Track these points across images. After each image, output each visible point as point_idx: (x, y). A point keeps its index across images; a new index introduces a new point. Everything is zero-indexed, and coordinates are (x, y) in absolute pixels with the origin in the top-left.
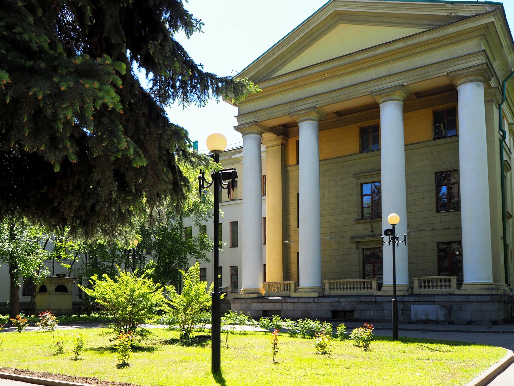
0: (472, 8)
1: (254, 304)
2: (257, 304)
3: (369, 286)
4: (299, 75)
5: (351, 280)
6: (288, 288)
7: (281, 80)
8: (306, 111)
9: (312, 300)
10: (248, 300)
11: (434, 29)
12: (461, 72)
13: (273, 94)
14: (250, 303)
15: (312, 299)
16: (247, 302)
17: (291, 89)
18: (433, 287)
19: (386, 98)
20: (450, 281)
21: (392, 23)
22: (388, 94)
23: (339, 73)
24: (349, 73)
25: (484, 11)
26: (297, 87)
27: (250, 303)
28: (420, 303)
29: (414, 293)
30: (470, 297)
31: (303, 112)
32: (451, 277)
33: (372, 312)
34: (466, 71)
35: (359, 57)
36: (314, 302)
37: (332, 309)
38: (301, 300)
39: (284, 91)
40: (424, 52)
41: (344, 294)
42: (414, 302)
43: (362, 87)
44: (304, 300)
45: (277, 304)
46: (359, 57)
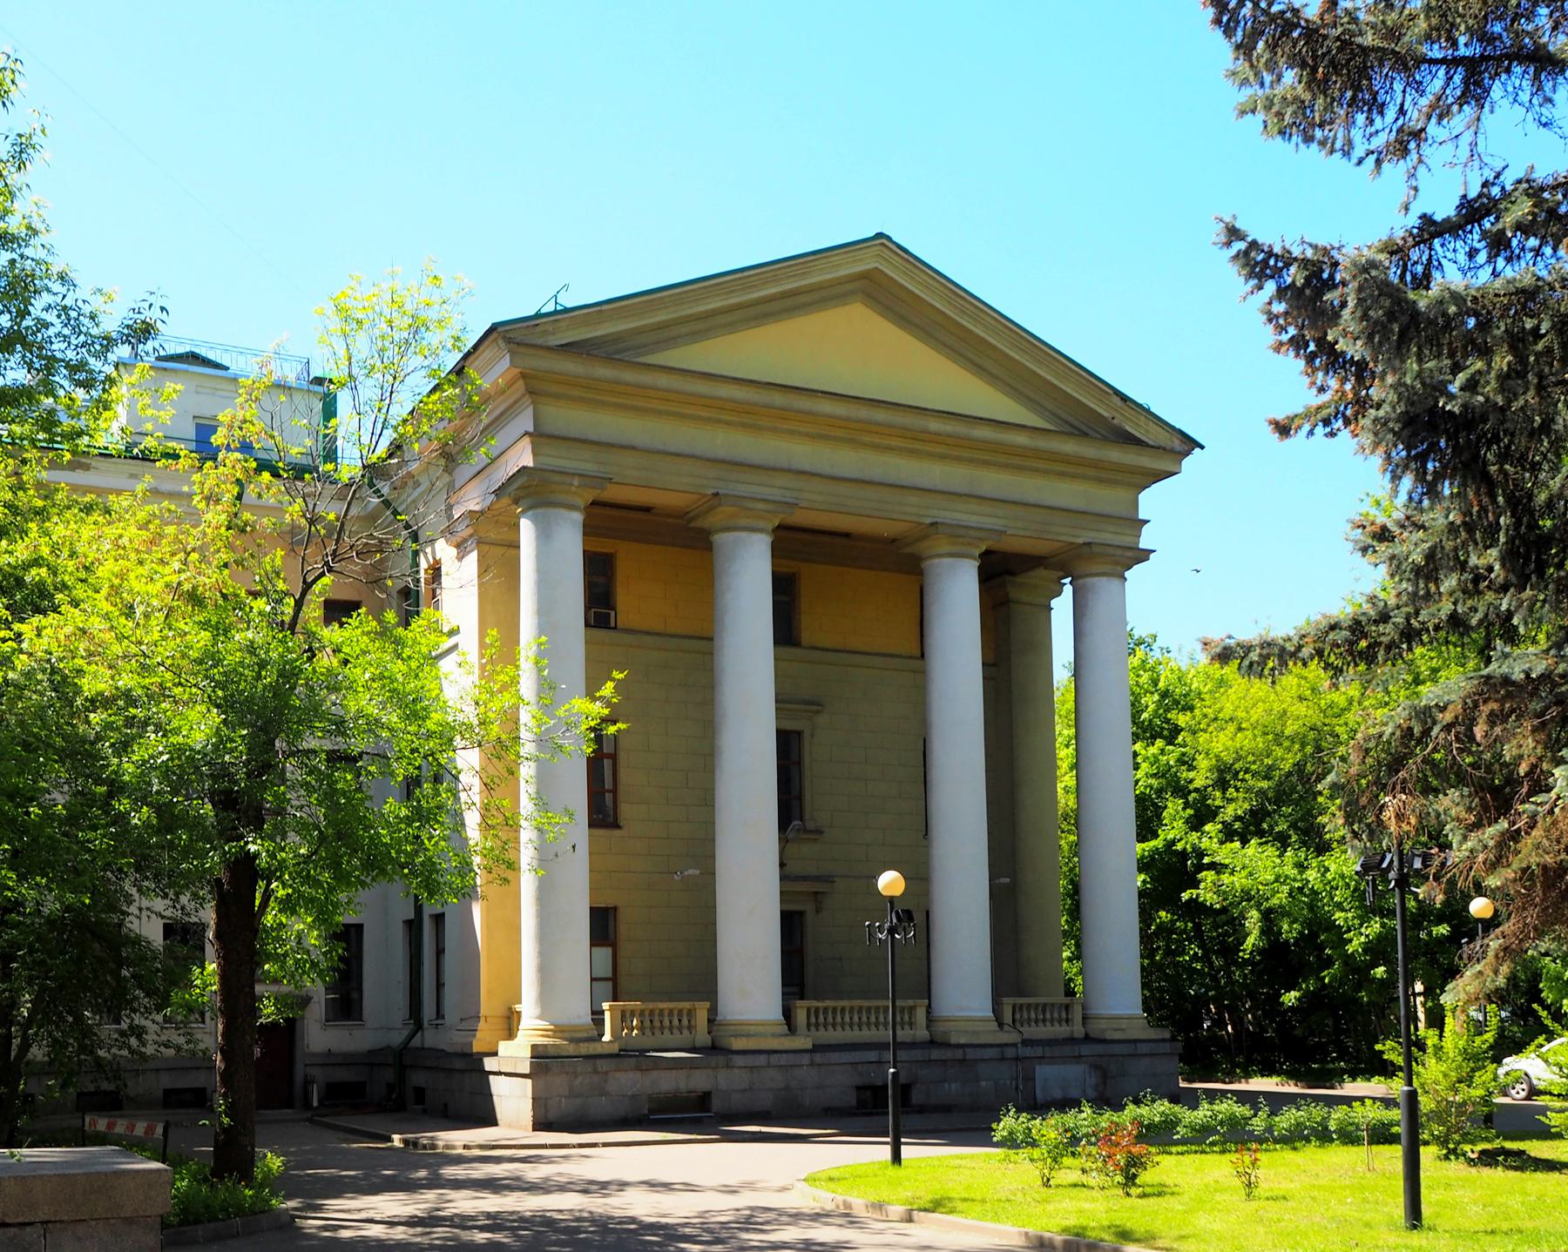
0: (1153, 427)
1: (618, 1075)
2: (631, 1075)
3: (685, 1022)
4: (778, 399)
5: (866, 1003)
6: (685, 1022)
7: (663, 380)
8: (770, 507)
9: (806, 1059)
10: (599, 1062)
11: (1071, 434)
12: (1112, 551)
13: (668, 413)
14: (606, 1073)
15: (807, 1056)
16: (595, 1071)
17: (728, 423)
18: (834, 1026)
19: (962, 549)
20: (691, 1013)
21: (984, 370)
22: (958, 536)
23: (867, 438)
24: (888, 449)
25: (1169, 444)
26: (744, 425)
27: (606, 1073)
28: (1053, 1060)
29: (1092, 1035)
30: (968, 1050)
31: (761, 506)
32: (698, 1004)
33: (953, 1086)
34: (1119, 552)
35: (935, 425)
36: (812, 1064)
37: (859, 1082)
38: (774, 1059)
39: (708, 420)
40: (1045, 472)
41: (848, 1041)
42: (1041, 1059)
43: (913, 499)
44: (784, 1059)
45: (697, 1073)
46: (935, 425)
